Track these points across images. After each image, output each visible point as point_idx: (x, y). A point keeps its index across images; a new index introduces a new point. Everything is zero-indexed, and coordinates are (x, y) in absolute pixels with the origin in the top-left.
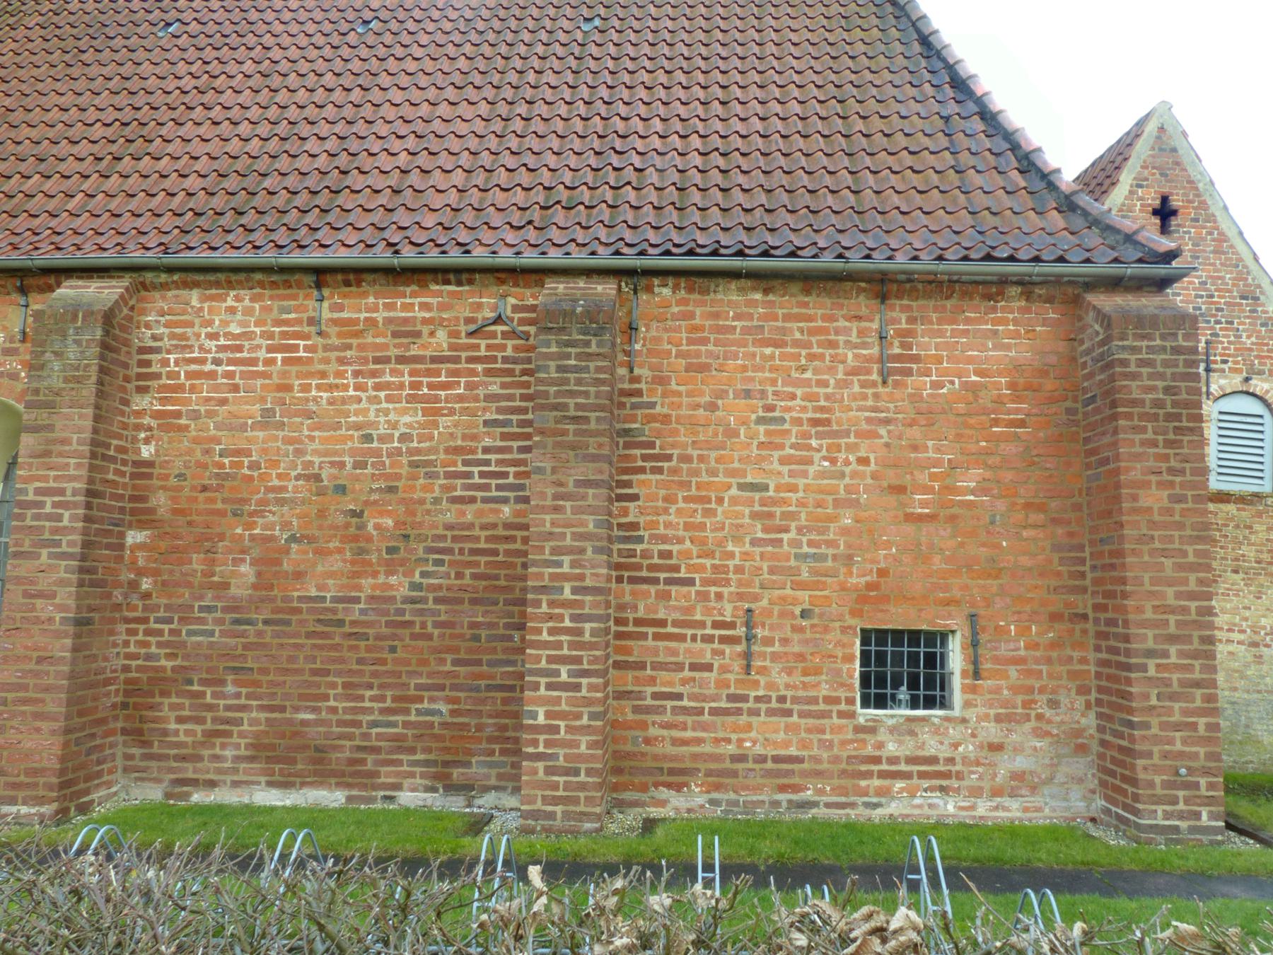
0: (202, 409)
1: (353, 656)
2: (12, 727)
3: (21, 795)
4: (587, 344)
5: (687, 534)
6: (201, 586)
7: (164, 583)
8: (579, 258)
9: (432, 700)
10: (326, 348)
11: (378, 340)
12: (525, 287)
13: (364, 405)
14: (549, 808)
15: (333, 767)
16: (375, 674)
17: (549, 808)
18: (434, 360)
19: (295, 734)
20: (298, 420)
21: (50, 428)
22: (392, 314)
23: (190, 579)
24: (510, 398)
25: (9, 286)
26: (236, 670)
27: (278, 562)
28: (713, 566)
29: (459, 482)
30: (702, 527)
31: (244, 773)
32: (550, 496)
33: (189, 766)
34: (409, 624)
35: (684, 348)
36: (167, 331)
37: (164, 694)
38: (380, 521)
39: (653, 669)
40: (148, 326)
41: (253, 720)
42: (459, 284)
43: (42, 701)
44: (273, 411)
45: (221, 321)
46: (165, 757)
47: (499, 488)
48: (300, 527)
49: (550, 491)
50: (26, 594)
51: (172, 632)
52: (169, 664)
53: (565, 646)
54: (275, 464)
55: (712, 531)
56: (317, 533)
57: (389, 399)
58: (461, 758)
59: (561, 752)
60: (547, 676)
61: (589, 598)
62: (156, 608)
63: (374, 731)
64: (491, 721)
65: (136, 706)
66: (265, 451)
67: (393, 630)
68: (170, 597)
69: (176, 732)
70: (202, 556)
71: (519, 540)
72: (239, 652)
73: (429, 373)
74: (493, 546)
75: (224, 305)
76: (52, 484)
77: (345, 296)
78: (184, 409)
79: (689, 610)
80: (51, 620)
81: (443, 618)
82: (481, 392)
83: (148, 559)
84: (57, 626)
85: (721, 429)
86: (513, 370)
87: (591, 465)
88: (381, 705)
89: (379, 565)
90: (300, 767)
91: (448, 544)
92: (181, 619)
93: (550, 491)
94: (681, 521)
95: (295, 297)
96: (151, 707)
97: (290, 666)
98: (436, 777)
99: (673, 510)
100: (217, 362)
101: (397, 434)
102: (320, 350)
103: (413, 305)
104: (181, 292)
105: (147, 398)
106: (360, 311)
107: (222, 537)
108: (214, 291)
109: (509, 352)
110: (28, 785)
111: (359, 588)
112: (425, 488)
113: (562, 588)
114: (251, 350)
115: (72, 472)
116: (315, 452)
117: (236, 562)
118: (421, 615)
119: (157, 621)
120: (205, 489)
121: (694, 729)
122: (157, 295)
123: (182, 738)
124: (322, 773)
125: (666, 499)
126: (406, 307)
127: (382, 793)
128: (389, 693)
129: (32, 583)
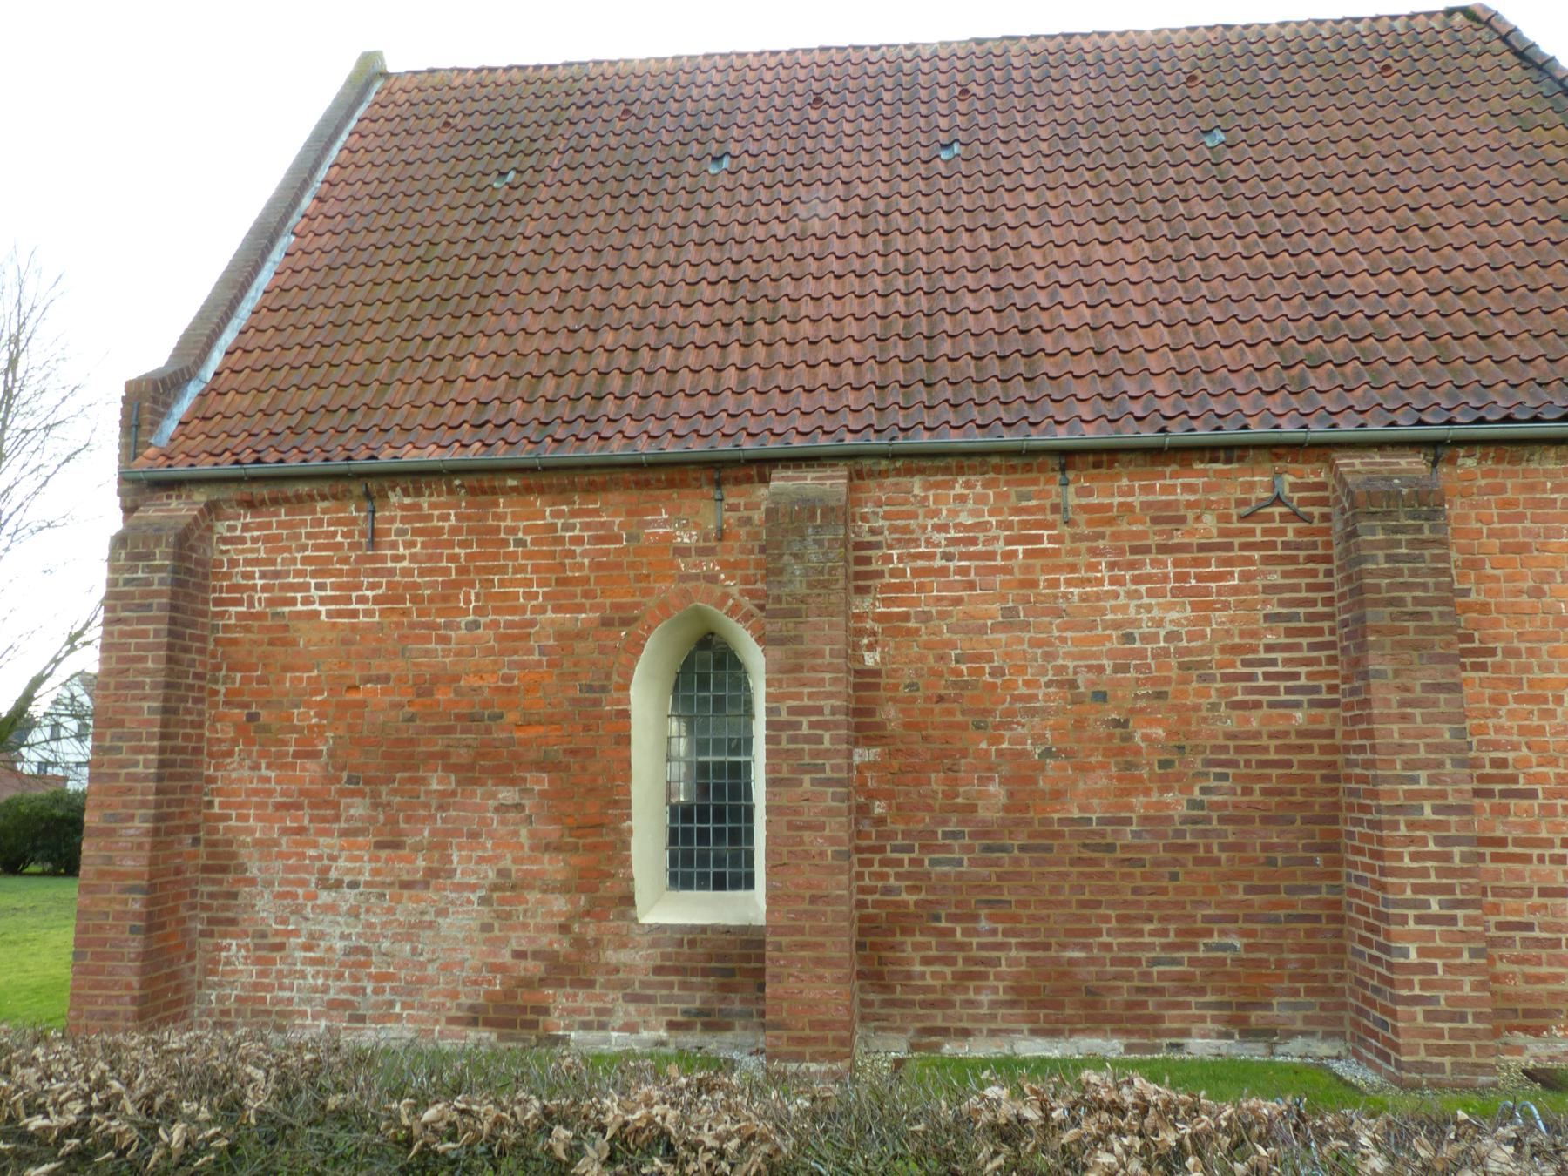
0: (934, 610)
1: (1127, 885)
2: (791, 975)
3: (808, 1050)
4: (1419, 529)
5: (1523, 740)
6: (943, 809)
7: (899, 807)
8: (1376, 430)
9: (1223, 933)
10: (1075, 538)
11: (1134, 528)
12: (1305, 462)
13: (1122, 600)
14: (1436, 1059)
15: (1108, 1011)
16: (1155, 905)
17: (1436, 1059)
18: (1202, 547)
19: (1064, 975)
20: (1047, 619)
21: (797, 639)
22: (1150, 498)
23: (930, 801)
24: (1295, 588)
25: (703, 478)
26: (989, 904)
27: (1032, 780)
28: (1558, 775)
29: (1240, 685)
30: (1540, 730)
31: (1004, 1020)
32: (1394, 703)
33: (938, 1013)
34: (1194, 847)
35: (1497, 526)
36: (886, 523)
37: (906, 931)
38: (1148, 731)
39: (1495, 895)
40: (864, 518)
41: (1012, 960)
42: (1228, 461)
43: (822, 945)
44: (1015, 609)
45: (949, 511)
46: (911, 1003)
47: (1289, 690)
48: (1054, 739)
49: (1395, 697)
50: (790, 826)
51: (912, 861)
52: (912, 898)
53: (1433, 873)
54: (1021, 670)
55: (1552, 735)
56: (1076, 747)
57: (1150, 593)
58: (1259, 998)
59: (1442, 994)
60: (1415, 907)
61: (1454, 818)
62: (891, 835)
63: (1156, 969)
64: (1293, 956)
65: (874, 946)
66: (1008, 655)
67: (1176, 855)
68: (907, 823)
69: (922, 975)
70: (942, 775)
71: (1316, 750)
72: (994, 882)
73: (1196, 563)
74: (1286, 757)
75: (952, 493)
76: (806, 702)
77: (1092, 479)
78: (912, 610)
79: (1533, 827)
80: (822, 854)
81: (1231, 839)
82: (1259, 582)
83: (880, 780)
84: (829, 860)
85: (1551, 617)
86: (1296, 557)
87: (1439, 667)
88: (1163, 940)
89: (1150, 780)
90: (1069, 1012)
91: (1231, 755)
92: (922, 847)
93: (1395, 697)
94: (1515, 724)
95: (1035, 482)
96: (892, 947)
97: (1053, 898)
98: (1231, 1021)
99: (1503, 711)
100: (948, 557)
101: (1162, 633)
102: (1068, 540)
103: (1174, 486)
104: (900, 480)
105: (868, 600)
106: (1113, 495)
107: (964, 754)
108: (940, 478)
109: (1290, 537)
110: (816, 1040)
111: (1130, 808)
112: (1198, 693)
113: (1422, 808)
114: (987, 542)
115: (828, 688)
116: (1068, 655)
117: (983, 781)
118: (1206, 837)
119: (895, 849)
120: (941, 699)
121: (1550, 964)
122: (872, 483)
123: (929, 981)
124: (1095, 1018)
125: (1493, 699)
126: (1167, 490)
127: (1168, 1041)
128: (1172, 927)
129: (797, 813)
